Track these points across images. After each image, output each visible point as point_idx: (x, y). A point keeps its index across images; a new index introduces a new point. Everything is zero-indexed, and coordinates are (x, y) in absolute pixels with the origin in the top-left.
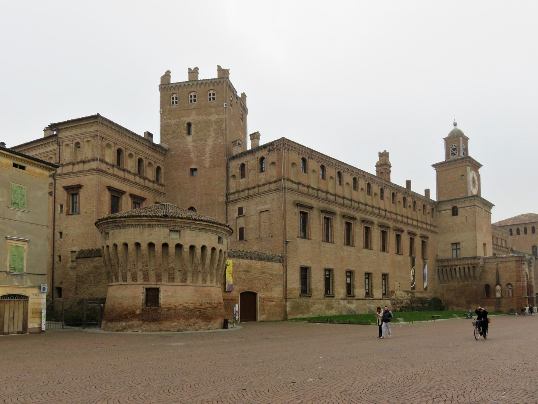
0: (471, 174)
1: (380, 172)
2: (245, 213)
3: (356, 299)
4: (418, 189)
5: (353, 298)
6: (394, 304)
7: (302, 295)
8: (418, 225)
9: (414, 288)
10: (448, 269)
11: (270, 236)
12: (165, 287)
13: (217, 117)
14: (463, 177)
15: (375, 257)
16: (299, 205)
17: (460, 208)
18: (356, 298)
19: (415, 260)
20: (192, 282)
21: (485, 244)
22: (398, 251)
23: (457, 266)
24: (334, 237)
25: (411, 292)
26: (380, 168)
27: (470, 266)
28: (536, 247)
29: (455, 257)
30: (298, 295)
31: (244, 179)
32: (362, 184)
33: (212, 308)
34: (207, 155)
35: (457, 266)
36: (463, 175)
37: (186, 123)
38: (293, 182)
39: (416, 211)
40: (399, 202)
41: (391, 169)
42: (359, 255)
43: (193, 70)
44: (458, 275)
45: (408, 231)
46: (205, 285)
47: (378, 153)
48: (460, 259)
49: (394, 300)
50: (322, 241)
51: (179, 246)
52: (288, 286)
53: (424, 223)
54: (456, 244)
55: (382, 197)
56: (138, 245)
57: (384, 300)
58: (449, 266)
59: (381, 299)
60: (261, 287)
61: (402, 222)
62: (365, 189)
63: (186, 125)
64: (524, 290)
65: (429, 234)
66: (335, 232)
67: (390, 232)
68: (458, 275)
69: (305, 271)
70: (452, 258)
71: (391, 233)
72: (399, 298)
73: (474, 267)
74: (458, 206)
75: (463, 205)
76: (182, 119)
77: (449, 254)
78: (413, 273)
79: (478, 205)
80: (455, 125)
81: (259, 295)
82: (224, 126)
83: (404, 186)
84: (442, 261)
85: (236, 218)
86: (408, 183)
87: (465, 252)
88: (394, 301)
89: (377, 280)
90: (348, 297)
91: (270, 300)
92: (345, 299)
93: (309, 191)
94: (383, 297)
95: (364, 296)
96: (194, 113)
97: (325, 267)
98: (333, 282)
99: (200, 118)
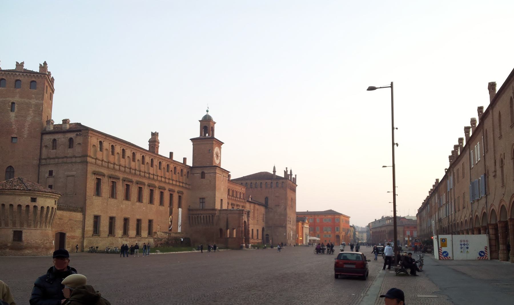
0: (216, 149)
1: (151, 146)
2: (55, 175)
3: (130, 238)
4: (178, 158)
5: (127, 237)
6: (155, 242)
7: (94, 235)
8: (177, 184)
9: (171, 230)
10: (196, 217)
11: (74, 194)
12: (25, 230)
13: (36, 101)
14: (210, 151)
15: (144, 208)
16: (94, 173)
17: (206, 173)
18: (129, 237)
19: (173, 210)
20: (40, 228)
21: (222, 200)
22: (161, 203)
23: (202, 214)
24: (117, 194)
25: (168, 233)
26: (151, 143)
27: (211, 216)
28: (268, 198)
29: (201, 208)
30: (92, 235)
31: (54, 151)
32: (138, 156)
33: (49, 243)
34: (26, 129)
35: (202, 214)
36: (210, 150)
37: (10, 102)
38: (93, 158)
39: (176, 174)
40: (164, 168)
41: (160, 145)
42: (133, 207)
43: (20, 63)
44: (202, 221)
45: (169, 189)
46: (46, 229)
47: (151, 133)
48: (206, 210)
49: (155, 238)
50: (109, 198)
51: (35, 207)
52: (86, 229)
53: (181, 182)
54: (203, 198)
55: (152, 165)
56: (11, 205)
57: (149, 239)
58: (196, 214)
59: (146, 238)
60: (68, 229)
61: (165, 182)
62: (140, 160)
63: (10, 104)
64: (242, 233)
65: (185, 191)
66: (118, 191)
67: (156, 190)
68: (202, 221)
69: (97, 219)
70: (199, 208)
71: (156, 191)
72: (159, 237)
73: (213, 216)
74: (206, 172)
75: (209, 172)
76: (7, 99)
77: (198, 206)
78: (171, 219)
79: (218, 173)
80: (207, 111)
81: (68, 234)
82: (41, 109)
83: (168, 156)
84: (192, 210)
85: (46, 177)
86: (171, 154)
87: (207, 206)
88: (156, 240)
89: (145, 225)
90: (125, 236)
91: (73, 238)
92: (122, 238)
93: (103, 164)
94: (148, 236)
95: (135, 236)
96: (18, 96)
97: (110, 215)
98: (114, 225)
99: (23, 100)
